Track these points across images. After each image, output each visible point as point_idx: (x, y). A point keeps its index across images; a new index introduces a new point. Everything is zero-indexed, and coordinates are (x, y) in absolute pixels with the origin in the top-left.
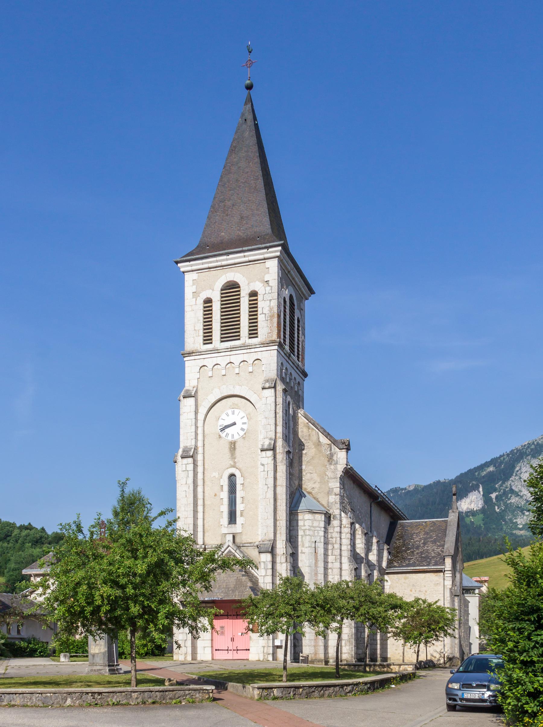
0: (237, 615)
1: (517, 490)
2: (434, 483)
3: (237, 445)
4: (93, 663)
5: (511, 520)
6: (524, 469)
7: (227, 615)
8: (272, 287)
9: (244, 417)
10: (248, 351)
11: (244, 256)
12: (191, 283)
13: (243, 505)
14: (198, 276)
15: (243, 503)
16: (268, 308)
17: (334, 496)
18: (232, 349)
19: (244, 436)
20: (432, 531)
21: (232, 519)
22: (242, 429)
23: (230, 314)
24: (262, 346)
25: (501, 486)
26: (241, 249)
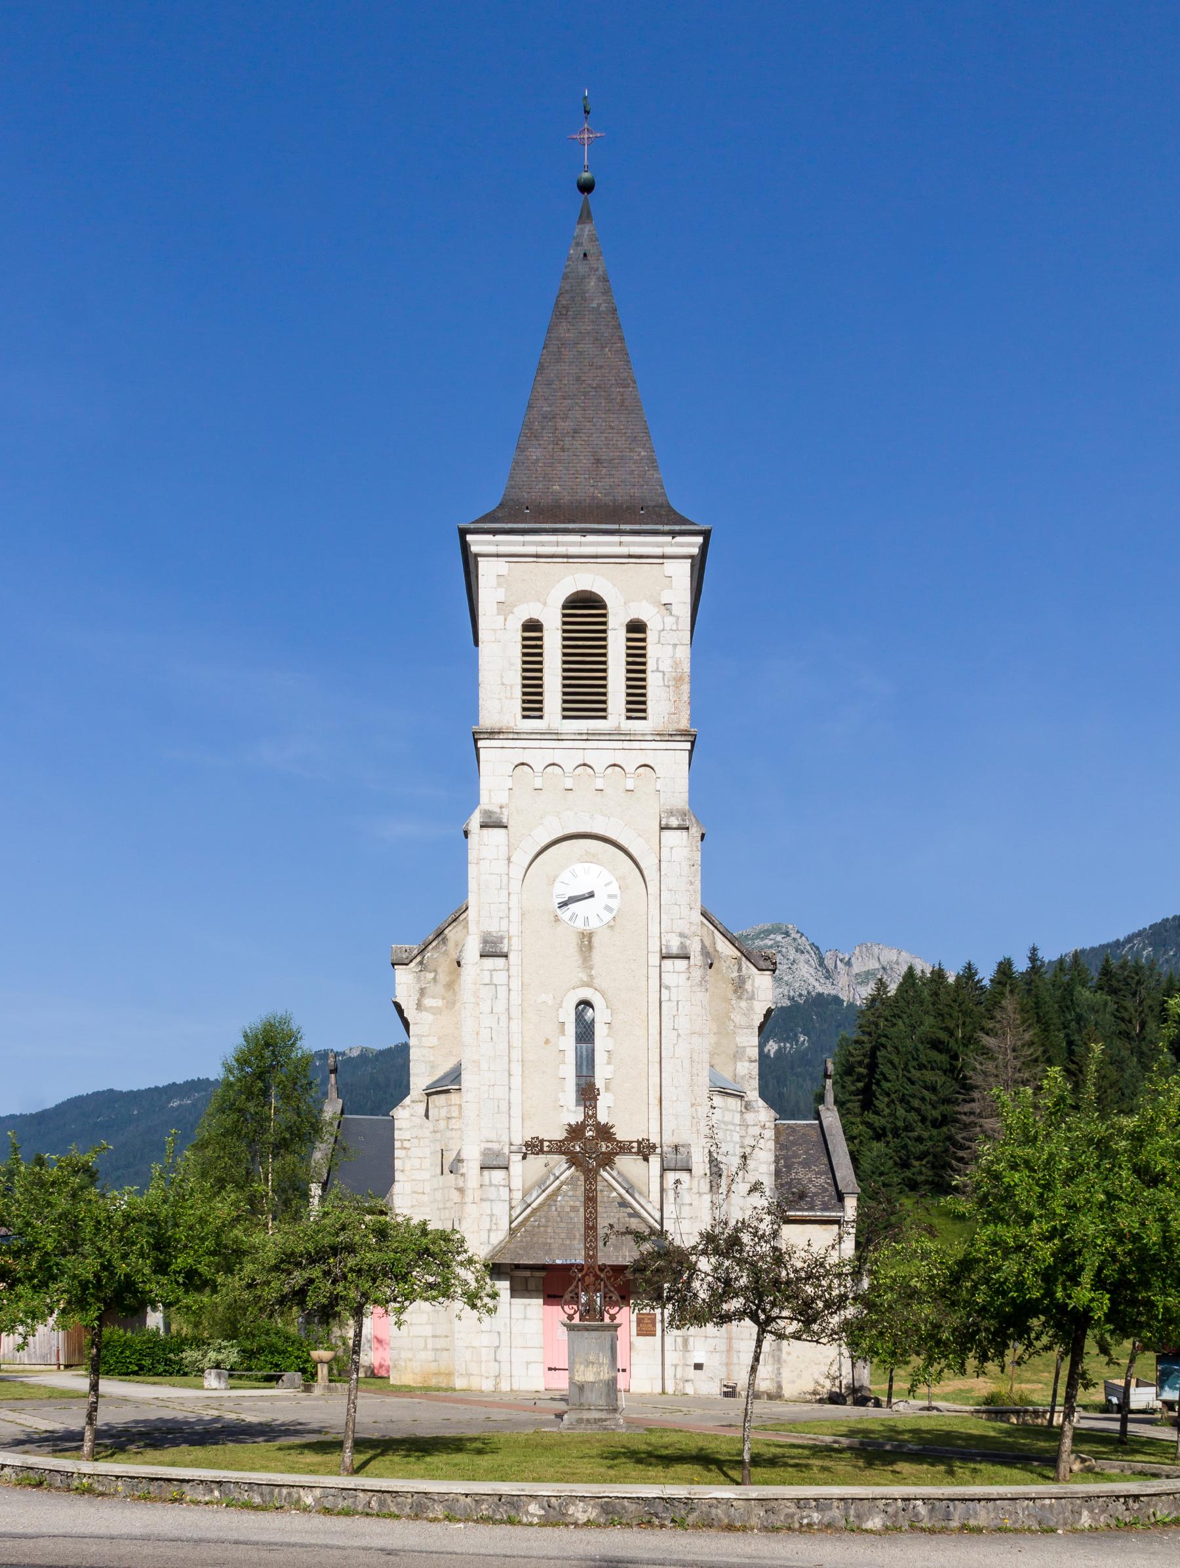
2: (397, 1046)
3: (595, 940)
4: (581, 1404)
8: (678, 618)
10: (626, 745)
13: (611, 1068)
14: (509, 569)
15: (609, 1063)
16: (669, 662)
17: (747, 1064)
18: (590, 736)
19: (612, 923)
20: (793, 1143)
22: (608, 909)
23: (584, 659)
24: (658, 738)
26: (616, 527)
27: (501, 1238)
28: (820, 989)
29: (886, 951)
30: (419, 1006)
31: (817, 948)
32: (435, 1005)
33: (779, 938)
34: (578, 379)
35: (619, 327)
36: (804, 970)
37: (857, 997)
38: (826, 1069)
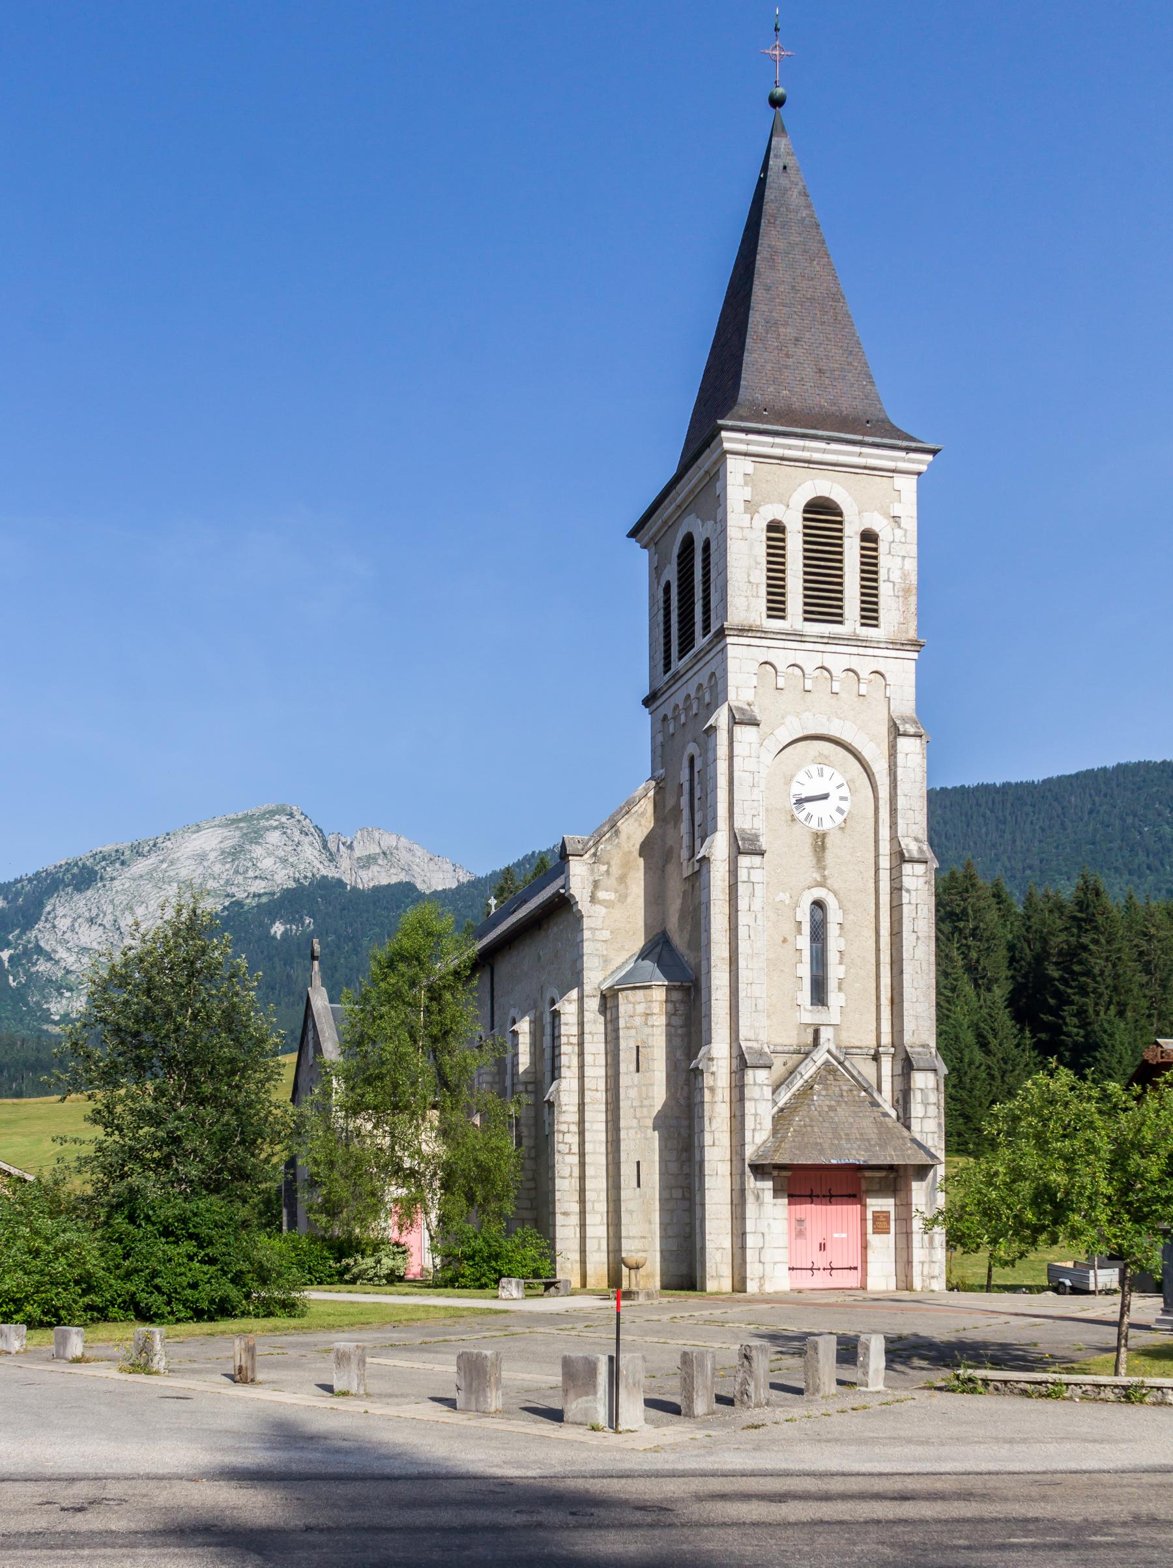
0: (831, 1196)
1: (48, 948)
3: (828, 841)
5: (38, 1003)
6: (60, 911)
7: (811, 1196)
8: (906, 531)
9: (842, 785)
10: (861, 651)
11: (860, 454)
12: (740, 479)
13: (843, 968)
15: (841, 963)
21: (819, 994)
22: (840, 810)
24: (891, 646)
25: (19, 937)
26: (859, 438)
27: (765, 1138)
28: (324, 872)
29: (386, 836)
30: (593, 899)
31: (321, 831)
32: (607, 898)
33: (284, 819)
34: (793, 287)
35: (823, 242)
36: (309, 852)
37: (359, 880)
38: (313, 951)
